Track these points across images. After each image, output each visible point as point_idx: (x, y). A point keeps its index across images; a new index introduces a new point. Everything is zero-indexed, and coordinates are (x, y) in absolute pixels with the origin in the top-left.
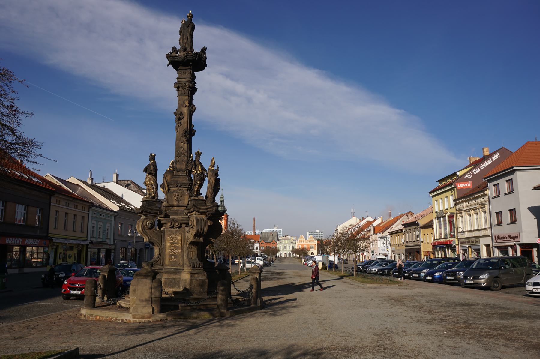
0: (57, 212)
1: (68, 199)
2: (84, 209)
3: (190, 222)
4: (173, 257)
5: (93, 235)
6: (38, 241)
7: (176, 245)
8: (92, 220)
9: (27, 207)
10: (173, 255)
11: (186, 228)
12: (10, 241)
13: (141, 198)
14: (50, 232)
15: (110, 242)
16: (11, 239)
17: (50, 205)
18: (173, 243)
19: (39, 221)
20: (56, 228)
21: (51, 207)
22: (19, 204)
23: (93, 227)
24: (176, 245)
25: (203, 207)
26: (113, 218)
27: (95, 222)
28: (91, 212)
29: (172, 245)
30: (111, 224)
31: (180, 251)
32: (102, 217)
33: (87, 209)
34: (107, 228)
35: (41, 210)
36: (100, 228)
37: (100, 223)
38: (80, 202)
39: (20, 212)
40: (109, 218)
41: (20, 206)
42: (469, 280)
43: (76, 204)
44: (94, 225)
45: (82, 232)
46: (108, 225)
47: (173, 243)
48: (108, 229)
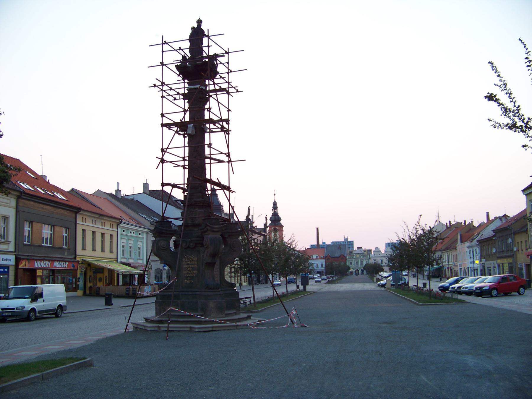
0: (84, 231)
1: (95, 216)
2: (112, 226)
3: (204, 242)
4: (189, 278)
5: (123, 255)
6: (67, 263)
7: (192, 266)
8: (121, 238)
9: (53, 227)
10: (190, 277)
11: (201, 248)
12: (39, 265)
13: (38, 275)
14: (77, 254)
15: (143, 261)
16: (39, 262)
17: (76, 223)
18: (188, 264)
19: (53, 261)
20: (84, 248)
21: (78, 225)
22: (45, 224)
23: (123, 246)
24: (192, 266)
25: (217, 226)
26: (145, 235)
27: (125, 241)
28: (119, 229)
29: (188, 266)
30: (142, 242)
31: (196, 272)
32: (132, 234)
33: (115, 226)
34: (139, 246)
35: (68, 229)
36: (130, 247)
37: (130, 242)
38: (107, 219)
39: (47, 231)
40: (140, 236)
41: (46, 226)
42: (43, 269)
43: (103, 221)
44: (124, 244)
45: (111, 251)
46: (139, 243)
47: (188, 264)
48: (139, 248)
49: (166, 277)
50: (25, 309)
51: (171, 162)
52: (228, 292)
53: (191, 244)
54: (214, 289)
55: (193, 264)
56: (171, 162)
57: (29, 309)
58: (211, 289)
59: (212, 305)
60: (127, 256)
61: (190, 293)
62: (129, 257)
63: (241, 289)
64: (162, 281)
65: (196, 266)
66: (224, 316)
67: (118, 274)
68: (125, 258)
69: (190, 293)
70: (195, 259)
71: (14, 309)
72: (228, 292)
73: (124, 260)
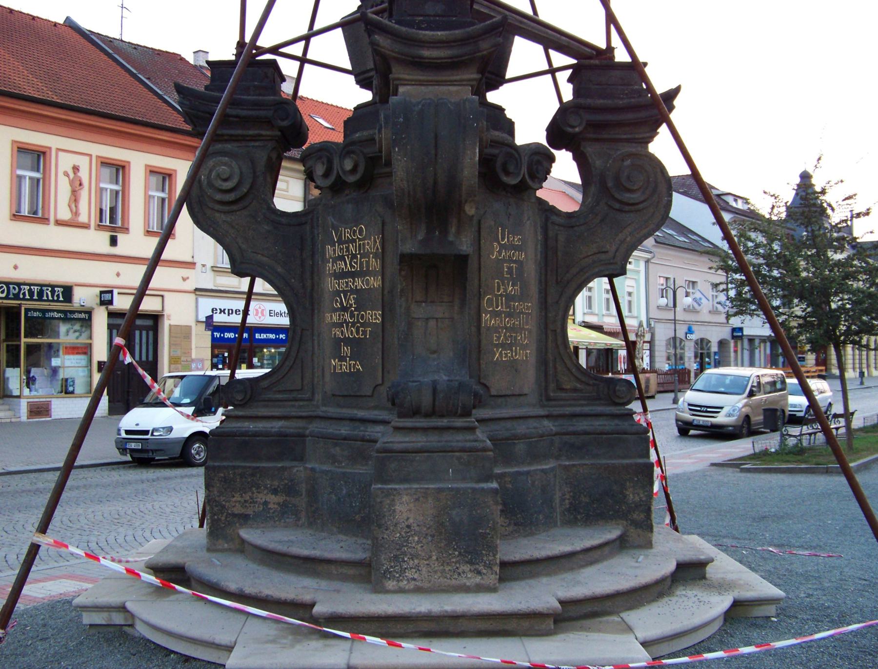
7: (359, 283)
10: (347, 341)
24: (359, 283)
26: (642, 265)
31: (374, 316)
48: (630, 294)
49: (692, 355)
50: (173, 435)
51: (611, 19)
52: (583, 425)
53: (348, 165)
54: (432, 413)
55: (361, 274)
56: (611, 19)
57: (187, 435)
58: (416, 412)
59: (407, 509)
60: (502, 300)
61: (344, 430)
62: (604, 312)
63: (862, 383)
64: (684, 364)
65: (375, 282)
66: (491, 579)
67: (576, 349)
68: (592, 314)
69: (344, 430)
70: (372, 244)
71: (146, 432)
72: (583, 425)
73: (592, 320)
